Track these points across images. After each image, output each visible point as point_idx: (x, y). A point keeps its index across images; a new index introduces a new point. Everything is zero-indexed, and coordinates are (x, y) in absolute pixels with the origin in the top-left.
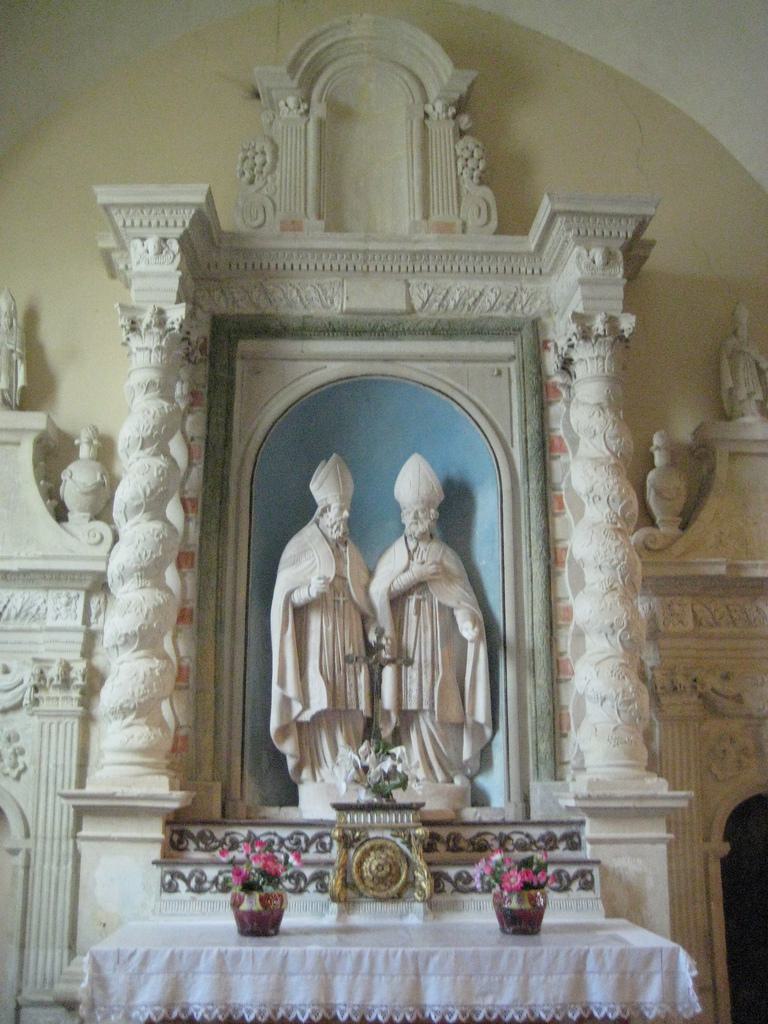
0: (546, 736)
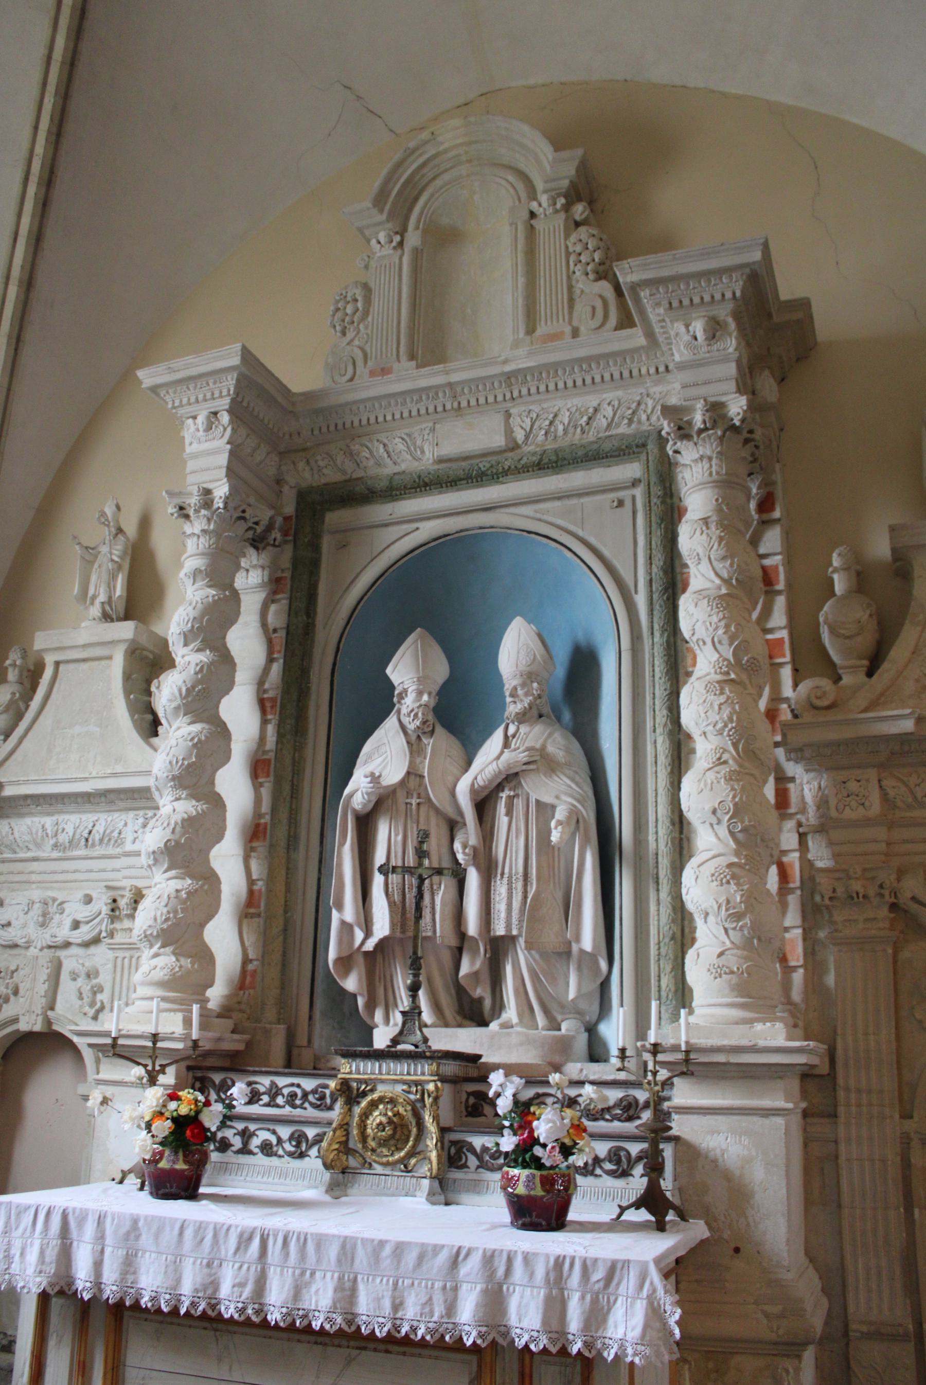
0: (668, 968)
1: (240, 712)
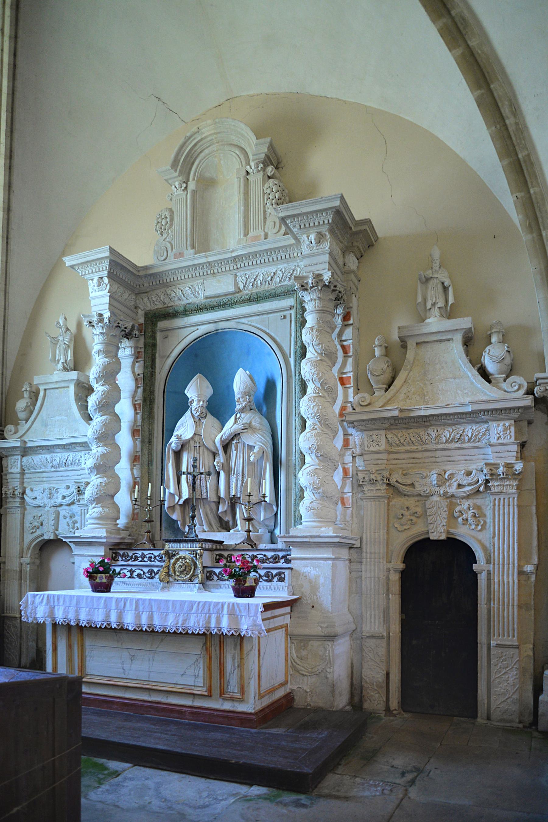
1: (125, 409)
